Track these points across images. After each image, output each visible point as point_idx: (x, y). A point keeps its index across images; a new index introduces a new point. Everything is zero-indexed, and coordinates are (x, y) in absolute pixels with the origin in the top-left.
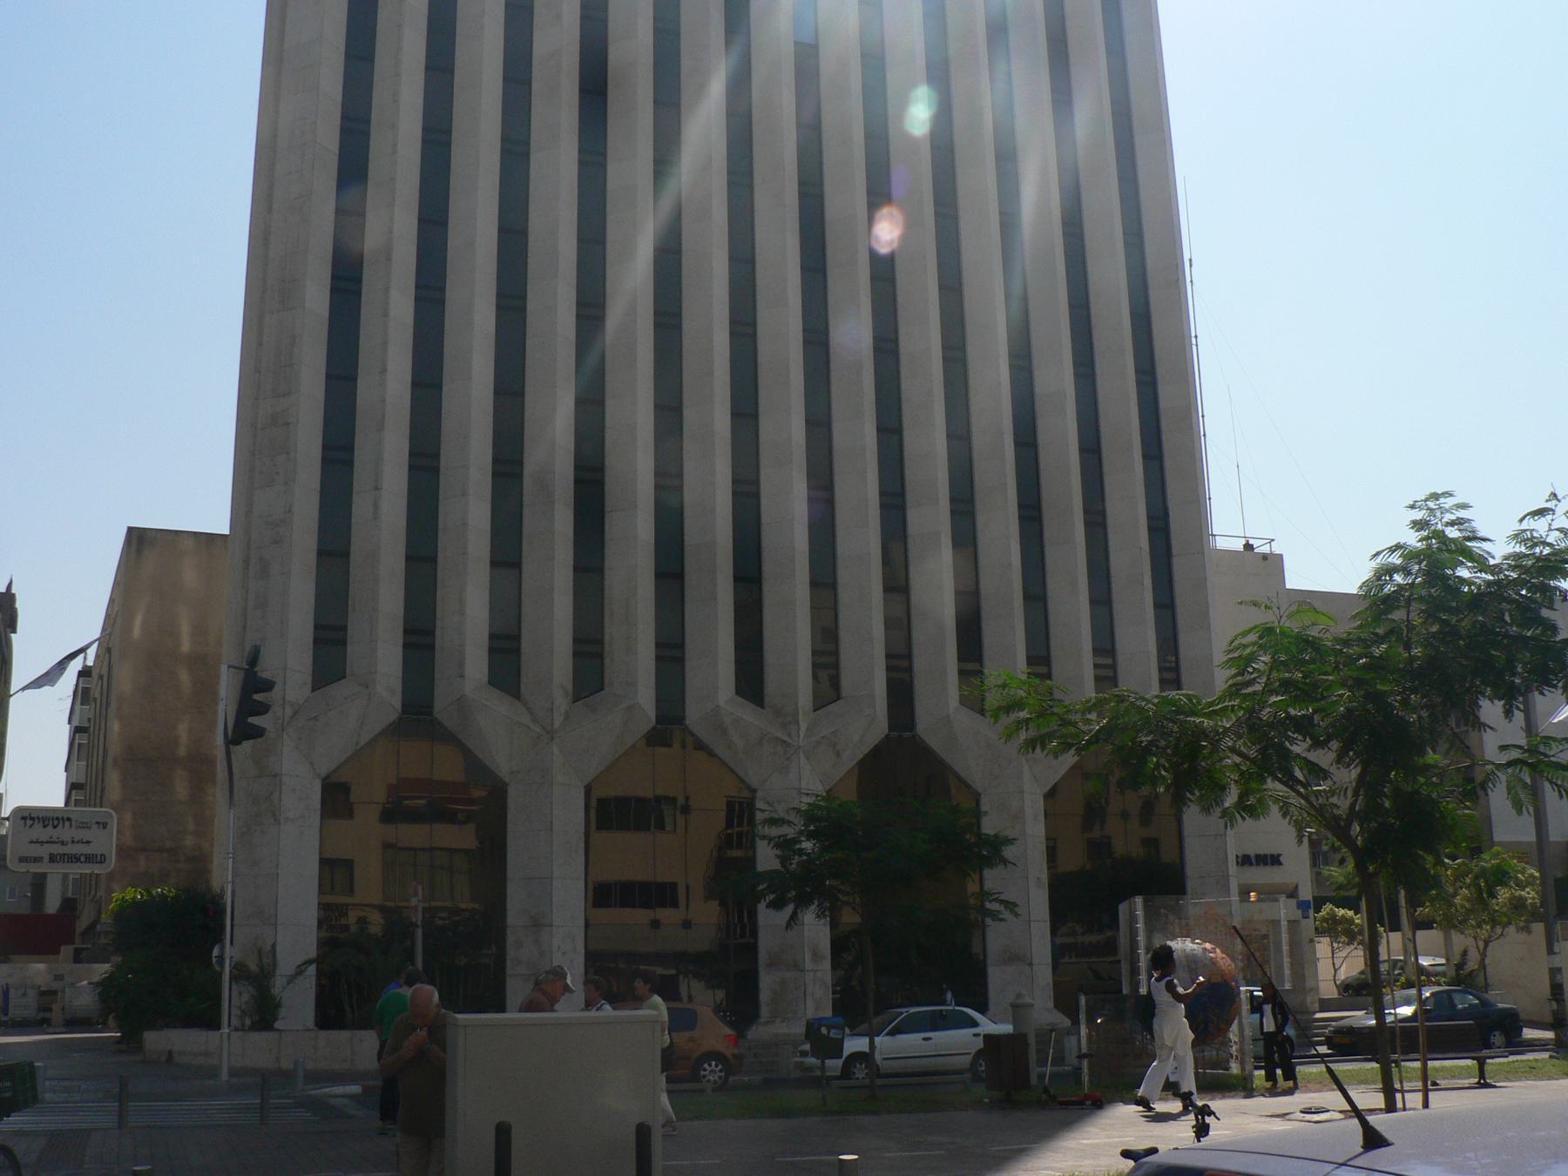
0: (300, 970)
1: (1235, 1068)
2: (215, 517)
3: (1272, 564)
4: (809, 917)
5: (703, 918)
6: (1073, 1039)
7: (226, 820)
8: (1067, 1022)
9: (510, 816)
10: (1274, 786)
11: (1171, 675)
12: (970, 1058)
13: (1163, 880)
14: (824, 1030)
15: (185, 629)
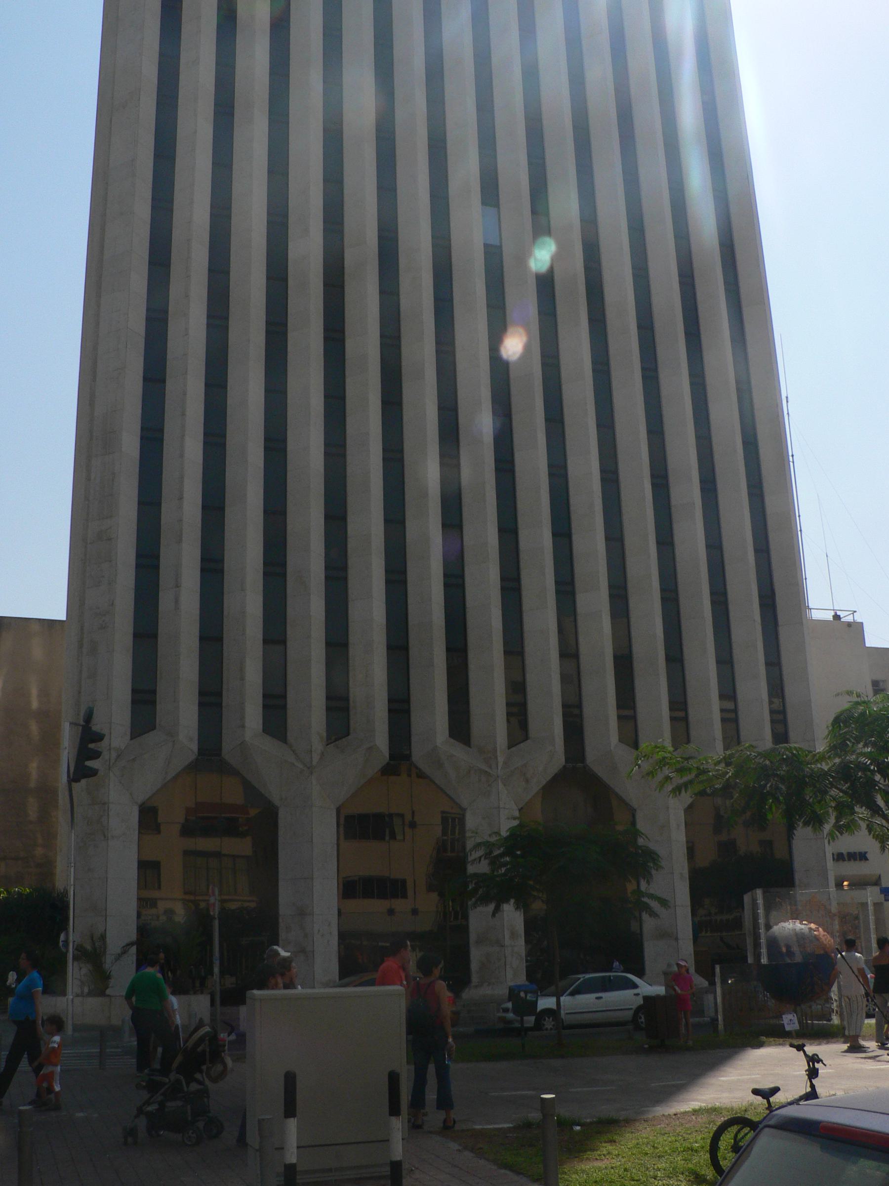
0: (125, 950)
1: (836, 1020)
2: (55, 608)
3: (856, 629)
4: (508, 908)
5: (423, 907)
6: (710, 997)
7: (66, 839)
8: (705, 983)
9: (281, 832)
10: (861, 811)
11: (781, 736)
12: (631, 1013)
13: (777, 876)
14: (522, 994)
15: (34, 692)
